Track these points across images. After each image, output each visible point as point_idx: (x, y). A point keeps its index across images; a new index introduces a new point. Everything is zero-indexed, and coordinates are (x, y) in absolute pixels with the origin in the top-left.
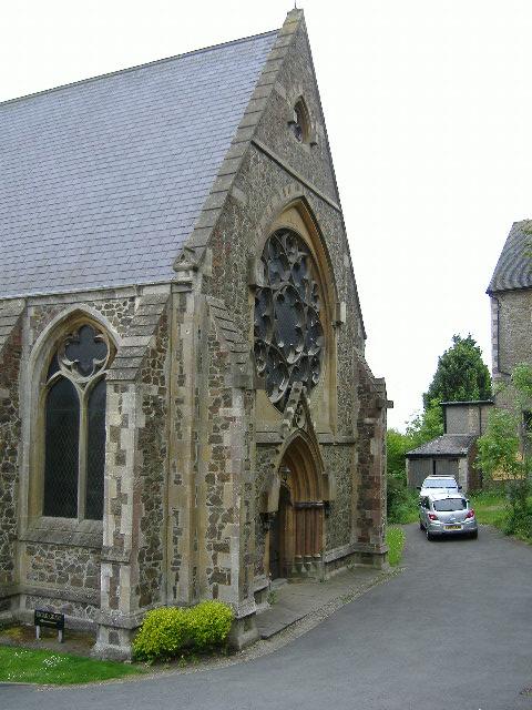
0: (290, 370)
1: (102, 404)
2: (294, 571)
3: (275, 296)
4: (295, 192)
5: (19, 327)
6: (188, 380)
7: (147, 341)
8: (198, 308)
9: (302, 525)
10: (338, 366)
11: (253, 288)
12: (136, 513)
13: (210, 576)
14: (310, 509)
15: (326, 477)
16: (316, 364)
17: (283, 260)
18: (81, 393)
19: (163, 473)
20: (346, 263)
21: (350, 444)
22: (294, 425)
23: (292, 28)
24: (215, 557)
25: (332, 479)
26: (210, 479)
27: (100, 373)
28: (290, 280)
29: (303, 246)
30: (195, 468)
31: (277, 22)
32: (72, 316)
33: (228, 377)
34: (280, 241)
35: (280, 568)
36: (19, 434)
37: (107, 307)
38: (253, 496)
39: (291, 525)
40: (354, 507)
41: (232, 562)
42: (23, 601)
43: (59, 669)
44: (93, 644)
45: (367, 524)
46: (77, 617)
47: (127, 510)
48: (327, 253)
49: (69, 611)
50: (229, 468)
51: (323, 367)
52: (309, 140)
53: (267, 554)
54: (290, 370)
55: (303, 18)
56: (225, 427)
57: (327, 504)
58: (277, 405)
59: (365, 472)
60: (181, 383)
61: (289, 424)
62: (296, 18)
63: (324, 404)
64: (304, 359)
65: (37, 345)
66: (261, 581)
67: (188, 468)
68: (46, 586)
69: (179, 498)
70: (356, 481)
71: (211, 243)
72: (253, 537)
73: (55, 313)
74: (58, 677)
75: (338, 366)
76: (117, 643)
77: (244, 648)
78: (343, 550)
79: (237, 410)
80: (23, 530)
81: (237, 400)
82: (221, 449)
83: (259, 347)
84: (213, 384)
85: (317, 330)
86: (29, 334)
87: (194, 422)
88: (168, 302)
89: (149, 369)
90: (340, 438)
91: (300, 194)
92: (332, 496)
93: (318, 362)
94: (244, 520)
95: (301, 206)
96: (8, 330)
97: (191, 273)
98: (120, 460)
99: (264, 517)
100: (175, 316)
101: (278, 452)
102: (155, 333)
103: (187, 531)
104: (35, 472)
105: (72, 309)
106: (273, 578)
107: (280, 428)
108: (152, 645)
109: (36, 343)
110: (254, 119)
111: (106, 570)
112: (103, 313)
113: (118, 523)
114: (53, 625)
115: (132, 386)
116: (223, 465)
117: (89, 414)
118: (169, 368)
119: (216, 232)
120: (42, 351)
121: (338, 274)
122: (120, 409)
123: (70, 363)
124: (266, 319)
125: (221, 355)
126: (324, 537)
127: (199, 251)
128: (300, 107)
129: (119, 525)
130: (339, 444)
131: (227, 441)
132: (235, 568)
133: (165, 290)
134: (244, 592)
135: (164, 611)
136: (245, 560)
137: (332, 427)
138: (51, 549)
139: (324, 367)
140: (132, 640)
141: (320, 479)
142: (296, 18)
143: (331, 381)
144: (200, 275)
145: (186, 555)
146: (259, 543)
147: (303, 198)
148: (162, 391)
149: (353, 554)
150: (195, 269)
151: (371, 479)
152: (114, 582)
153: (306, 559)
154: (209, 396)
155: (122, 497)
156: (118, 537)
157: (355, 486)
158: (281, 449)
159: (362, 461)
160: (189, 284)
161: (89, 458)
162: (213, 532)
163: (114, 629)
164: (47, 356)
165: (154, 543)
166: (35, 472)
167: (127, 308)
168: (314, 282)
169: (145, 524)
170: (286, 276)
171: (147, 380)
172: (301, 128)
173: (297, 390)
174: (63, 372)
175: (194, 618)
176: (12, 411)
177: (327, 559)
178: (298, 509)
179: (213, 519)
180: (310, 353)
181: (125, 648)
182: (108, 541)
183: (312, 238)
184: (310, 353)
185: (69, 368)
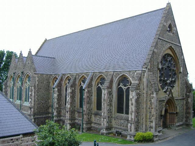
0: (168, 84)
1: (129, 95)
3: (164, 69)
4: (169, 45)
5: (112, 77)
6: (145, 90)
7: (137, 82)
8: (147, 75)
9: (171, 117)
10: (180, 82)
11: (159, 69)
12: (135, 114)
15: (176, 107)
16: (175, 81)
17: (166, 60)
18: (124, 90)
21: (183, 99)
22: (169, 96)
23: (168, 8)
24: (150, 124)
25: (178, 107)
26: (149, 108)
27: (128, 87)
28: (168, 64)
30: (146, 106)
31: (164, 6)
32: (122, 75)
33: (153, 89)
34: (165, 57)
35: (165, 126)
36: (112, 98)
38: (158, 112)
39: (168, 117)
40: (184, 113)
41: (153, 124)
42: (113, 129)
43: (121, 141)
44: (127, 138)
45: (187, 118)
46: (123, 132)
47: (133, 114)
48: (177, 57)
49: (122, 131)
50: (153, 107)
51: (176, 82)
54: (168, 84)
55: (170, 5)
56: (152, 98)
57: (177, 113)
58: (165, 92)
59: (187, 106)
60: (144, 90)
61: (167, 96)
62: (169, 5)
63: (176, 91)
64: (172, 81)
65: (116, 80)
66: (161, 129)
67: (145, 106)
68: (117, 126)
69: (143, 112)
70: (185, 107)
71: (150, 62)
72: (158, 120)
73: (119, 75)
74: (121, 142)
75: (180, 82)
76: (131, 138)
77: (156, 141)
78: (181, 123)
79: (154, 95)
80: (113, 116)
81: (155, 94)
83: (160, 80)
84: (150, 90)
86: (114, 78)
88: (141, 74)
89: (138, 87)
90: (180, 98)
91: (170, 45)
92: (178, 111)
94: (156, 116)
95: (171, 48)
96: (111, 78)
98: (132, 104)
99: (161, 116)
102: (139, 81)
103: (144, 118)
104: (116, 105)
106: (163, 128)
107: (163, 96)
108: (138, 139)
109: (116, 80)
110: (159, 33)
111: (129, 125)
114: (119, 134)
115: (134, 91)
116: (152, 106)
117: (126, 94)
118: (141, 87)
119: (151, 59)
120: (117, 81)
121: (180, 61)
124: (162, 74)
125: (152, 84)
126: (176, 120)
127: (147, 64)
128: (170, 26)
129: (132, 116)
130: (180, 99)
131: (153, 101)
132: (154, 126)
133: (141, 72)
134: (156, 130)
135: (140, 133)
136: (156, 124)
137: (179, 96)
139: (177, 82)
140: (134, 138)
142: (169, 5)
143: (178, 85)
146: (160, 121)
147: (171, 46)
148: (140, 91)
149: (184, 124)
150: (146, 68)
151: (188, 107)
152: (131, 127)
153: (172, 125)
154: (149, 92)
155: (132, 111)
156: (132, 118)
157: (185, 109)
158: (165, 101)
159: (186, 103)
161: (126, 102)
162: (150, 119)
163: (131, 135)
165: (138, 120)
166: (116, 105)
168: (174, 63)
169: (137, 117)
170: (167, 64)
171: (137, 90)
172: (170, 31)
174: (121, 86)
175: (145, 134)
176: (111, 93)
177: (177, 125)
178: (170, 114)
179: (150, 116)
180: (173, 79)
181: (132, 139)
182: (130, 119)
183: (173, 54)
184: (173, 79)
185: (122, 85)
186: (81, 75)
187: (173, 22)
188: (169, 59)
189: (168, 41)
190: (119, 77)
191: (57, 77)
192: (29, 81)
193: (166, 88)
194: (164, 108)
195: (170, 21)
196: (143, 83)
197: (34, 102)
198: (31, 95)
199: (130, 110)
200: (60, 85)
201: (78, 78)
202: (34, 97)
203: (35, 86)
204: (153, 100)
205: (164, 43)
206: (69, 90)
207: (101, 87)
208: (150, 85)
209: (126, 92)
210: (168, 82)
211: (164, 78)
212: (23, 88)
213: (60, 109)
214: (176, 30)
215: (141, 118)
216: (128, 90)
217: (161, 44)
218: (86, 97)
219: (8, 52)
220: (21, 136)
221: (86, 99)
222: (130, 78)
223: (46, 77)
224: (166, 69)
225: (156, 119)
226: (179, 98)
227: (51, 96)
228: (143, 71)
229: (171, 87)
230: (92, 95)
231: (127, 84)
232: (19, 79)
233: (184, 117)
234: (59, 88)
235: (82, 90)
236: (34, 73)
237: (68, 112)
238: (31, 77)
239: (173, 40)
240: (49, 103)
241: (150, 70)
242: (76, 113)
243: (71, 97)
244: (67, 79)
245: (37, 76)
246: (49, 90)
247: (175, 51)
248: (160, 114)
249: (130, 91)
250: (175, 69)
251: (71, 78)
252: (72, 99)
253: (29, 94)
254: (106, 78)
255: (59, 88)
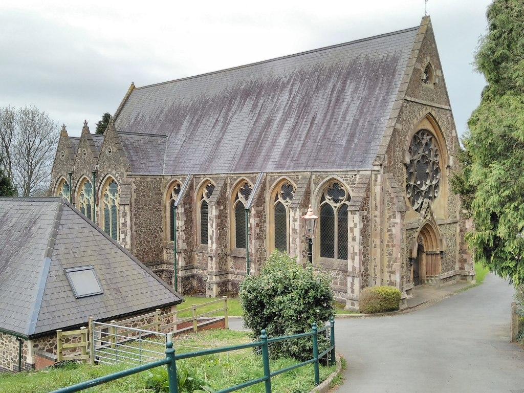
2: (426, 282)
3: (415, 162)
4: (425, 112)
5: (309, 184)
6: (379, 208)
9: (430, 262)
11: (405, 164)
13: (388, 283)
14: (434, 254)
15: (441, 240)
16: (437, 186)
17: (420, 143)
18: (335, 210)
19: (369, 244)
20: (454, 135)
22: (425, 218)
24: (390, 276)
27: (342, 203)
28: (423, 152)
29: (429, 133)
32: (330, 180)
37: (345, 177)
40: (457, 252)
47: (357, 258)
50: (395, 242)
52: (433, 82)
53: (412, 274)
55: (430, 21)
56: (394, 226)
58: (416, 210)
60: (376, 209)
62: (426, 19)
64: (430, 186)
71: (387, 152)
72: (405, 269)
76: (354, 306)
81: (398, 216)
82: (392, 235)
83: (407, 187)
84: (389, 209)
85: (437, 171)
86: (313, 186)
87: (381, 225)
93: (438, 186)
97: (379, 166)
98: (354, 239)
99: (411, 259)
100: (373, 183)
101: (417, 231)
105: (330, 177)
107: (417, 220)
109: (315, 191)
111: (349, 279)
112: (343, 180)
113: (353, 262)
115: (358, 213)
116: (393, 241)
118: (371, 203)
122: (353, 221)
123: (330, 198)
124: (411, 173)
125: (391, 198)
128: (428, 70)
129: (353, 263)
132: (398, 280)
138: (325, 270)
139: (441, 187)
141: (438, 241)
142: (426, 19)
144: (383, 166)
145: (378, 275)
146: (408, 270)
147: (430, 113)
152: (352, 284)
155: (355, 254)
156: (354, 268)
157: (458, 244)
158: (419, 230)
159: (461, 231)
160: (378, 171)
161: (339, 225)
162: (389, 266)
164: (321, 195)
165: (367, 270)
167: (353, 178)
169: (363, 263)
173: (426, 203)
174: (327, 201)
179: (389, 261)
182: (350, 269)
183: (435, 131)
185: (330, 199)
186: (238, 177)
187: (435, 59)
188: (426, 138)
189: (423, 102)
190: (322, 183)
191: (179, 181)
192: (114, 191)
193: (420, 201)
194: (417, 244)
195: (429, 58)
196: (373, 196)
197: (131, 239)
198: (123, 224)
199: (350, 251)
200: (188, 199)
201: (231, 185)
202: (131, 228)
203: (131, 203)
204: (394, 230)
205: (416, 107)
206: (214, 211)
207: (285, 204)
208: (387, 198)
209: (338, 215)
210: (424, 188)
211: (415, 182)
212: (97, 209)
213: (192, 251)
214: (440, 75)
215: (371, 266)
216: (343, 211)
217: (409, 112)
218: (253, 226)
219: (25, 113)
220: (158, 311)
221: (253, 230)
222: (347, 185)
223: (152, 181)
224: (419, 161)
225: (402, 267)
226: (445, 222)
227: (166, 225)
228: (374, 171)
229: (430, 198)
230: (265, 222)
231: (341, 198)
232: (83, 188)
233: (457, 260)
234: (187, 206)
235: (241, 211)
236: (128, 175)
237: (212, 260)
238: (121, 184)
239: (433, 100)
240: (161, 240)
241: (387, 169)
242: (229, 258)
243: (218, 225)
244: (205, 185)
245: (133, 180)
246: (161, 211)
247: (437, 123)
248: (407, 256)
249: (349, 213)
250: (438, 159)
251: (215, 185)
252: (219, 229)
253: (115, 224)
254: (295, 186)
255: (187, 206)
